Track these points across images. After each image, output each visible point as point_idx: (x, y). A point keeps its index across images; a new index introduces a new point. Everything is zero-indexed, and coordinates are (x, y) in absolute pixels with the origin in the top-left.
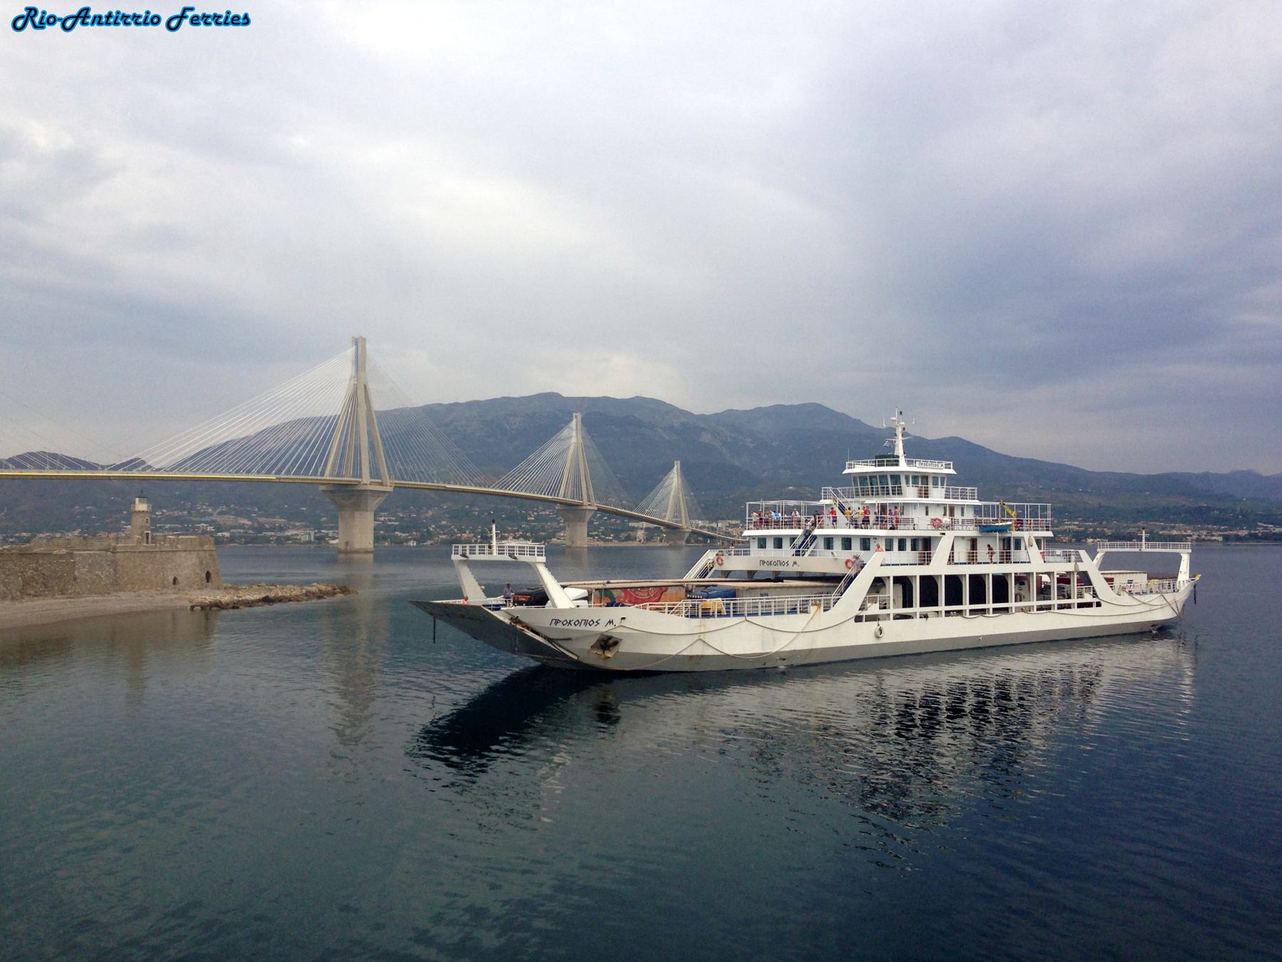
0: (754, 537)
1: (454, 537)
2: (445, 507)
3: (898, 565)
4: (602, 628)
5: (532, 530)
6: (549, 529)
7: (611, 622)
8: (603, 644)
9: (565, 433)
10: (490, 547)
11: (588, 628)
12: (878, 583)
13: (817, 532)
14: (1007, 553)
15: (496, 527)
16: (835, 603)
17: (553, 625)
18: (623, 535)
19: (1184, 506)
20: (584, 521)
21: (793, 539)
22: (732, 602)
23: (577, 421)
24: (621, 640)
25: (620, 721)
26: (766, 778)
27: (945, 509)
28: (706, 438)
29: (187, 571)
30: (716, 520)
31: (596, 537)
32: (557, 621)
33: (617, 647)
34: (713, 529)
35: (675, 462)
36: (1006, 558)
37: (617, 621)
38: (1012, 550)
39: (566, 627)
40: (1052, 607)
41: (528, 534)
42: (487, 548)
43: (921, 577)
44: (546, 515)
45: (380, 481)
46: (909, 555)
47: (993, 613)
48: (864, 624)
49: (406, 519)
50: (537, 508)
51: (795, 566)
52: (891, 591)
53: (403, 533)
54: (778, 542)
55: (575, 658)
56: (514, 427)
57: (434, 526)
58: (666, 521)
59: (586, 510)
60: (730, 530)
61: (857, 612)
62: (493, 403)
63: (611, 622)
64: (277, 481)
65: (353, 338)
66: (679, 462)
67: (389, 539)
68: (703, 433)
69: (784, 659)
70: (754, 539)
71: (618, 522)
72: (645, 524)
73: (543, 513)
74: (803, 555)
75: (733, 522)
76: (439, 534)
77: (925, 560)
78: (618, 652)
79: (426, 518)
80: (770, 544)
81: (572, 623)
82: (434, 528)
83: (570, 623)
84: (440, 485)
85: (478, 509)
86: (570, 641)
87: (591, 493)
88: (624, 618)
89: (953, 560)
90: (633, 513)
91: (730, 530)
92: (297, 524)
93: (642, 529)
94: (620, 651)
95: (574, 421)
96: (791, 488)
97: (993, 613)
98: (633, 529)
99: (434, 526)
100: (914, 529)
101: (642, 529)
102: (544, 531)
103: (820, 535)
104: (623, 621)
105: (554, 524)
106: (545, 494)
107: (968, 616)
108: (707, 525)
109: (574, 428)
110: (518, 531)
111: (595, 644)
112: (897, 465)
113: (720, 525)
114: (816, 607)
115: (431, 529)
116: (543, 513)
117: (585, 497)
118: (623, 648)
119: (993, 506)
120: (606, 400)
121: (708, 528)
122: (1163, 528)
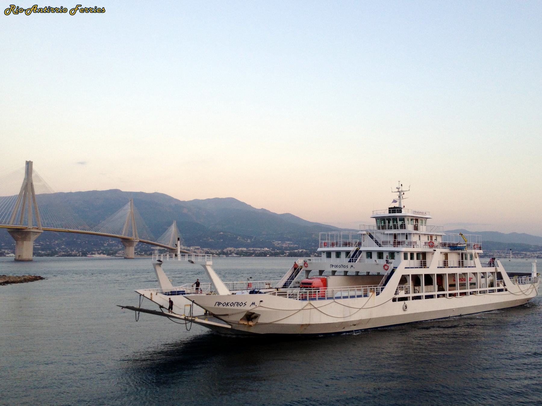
0: (324, 252)
1: (69, 253)
2: (64, 240)
3: (409, 268)
4: (248, 308)
5: (106, 250)
6: (113, 250)
7: (253, 304)
8: (248, 317)
10: (176, 255)
11: (239, 307)
12: (403, 280)
13: (362, 249)
14: (424, 261)
15: (180, 242)
16: (382, 290)
17: (217, 306)
18: (148, 253)
20: (133, 246)
21: (348, 253)
22: (308, 291)
23: (131, 203)
24: (260, 315)
27: (428, 236)
28: (185, 211)
30: (189, 246)
31: (136, 254)
32: (219, 304)
33: (256, 319)
34: (189, 250)
35: (174, 221)
36: (461, 264)
37: (257, 303)
38: (464, 260)
39: (225, 307)
40: (486, 292)
42: (174, 255)
43: (425, 275)
44: (112, 244)
45: (37, 227)
46: (416, 262)
47: (460, 295)
48: (397, 303)
49: (44, 245)
50: (109, 240)
51: (352, 268)
52: (410, 283)
53: (43, 251)
54: (338, 254)
55: (230, 327)
57: (58, 248)
58: (169, 246)
59: (134, 241)
60: (196, 250)
61: (393, 296)
62: (89, 193)
63: (253, 304)
66: (175, 221)
67: (36, 254)
69: (355, 325)
70: (324, 252)
72: (158, 248)
73: (111, 242)
74: (355, 262)
76: (60, 252)
77: (424, 265)
78: (257, 322)
80: (333, 255)
81: (229, 304)
82: (58, 249)
83: (227, 304)
84: (66, 229)
86: (227, 316)
87: (137, 234)
88: (261, 301)
89: (463, 265)
90: (155, 243)
91: (196, 250)
93: (157, 250)
94: (258, 322)
96: (222, 233)
97: (460, 295)
98: (153, 250)
99: (58, 248)
100: (414, 247)
101: (157, 250)
102: (112, 251)
103: (363, 251)
104: (261, 303)
105: (117, 248)
107: (448, 297)
110: (99, 251)
111: (243, 317)
112: (401, 212)
113: (191, 248)
114: (372, 293)
115: (57, 250)
116: (111, 242)
117: (134, 236)
118: (260, 320)
119: (469, 236)
120: (141, 193)
121: (186, 250)
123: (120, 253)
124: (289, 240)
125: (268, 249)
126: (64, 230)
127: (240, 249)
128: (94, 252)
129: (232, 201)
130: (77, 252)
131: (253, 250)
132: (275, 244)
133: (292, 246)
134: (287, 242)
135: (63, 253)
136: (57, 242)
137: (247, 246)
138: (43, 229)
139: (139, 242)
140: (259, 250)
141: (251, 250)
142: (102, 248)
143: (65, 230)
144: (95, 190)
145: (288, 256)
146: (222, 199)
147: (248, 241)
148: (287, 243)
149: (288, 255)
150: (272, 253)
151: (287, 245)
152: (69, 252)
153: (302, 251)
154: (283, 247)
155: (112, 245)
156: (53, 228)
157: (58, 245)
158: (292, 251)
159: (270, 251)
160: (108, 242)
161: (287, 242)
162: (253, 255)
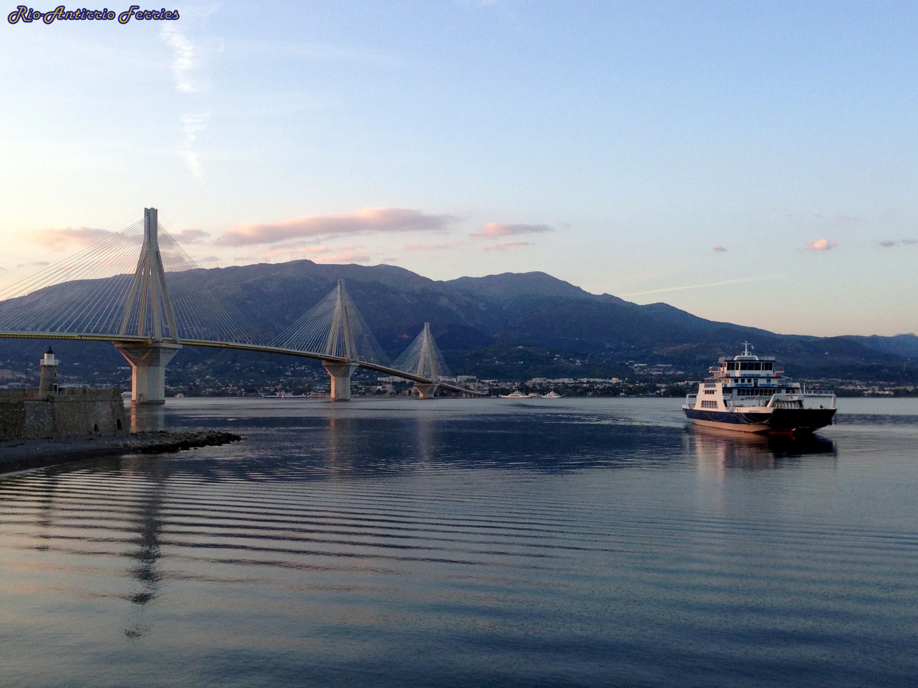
9: (332, 295)
19: (859, 364)
20: (348, 376)
25: (151, 601)
26: (774, 511)
28: (443, 302)
29: (104, 419)
30: (455, 375)
35: (425, 323)
41: (288, 387)
50: (294, 365)
53: (172, 386)
56: (271, 291)
58: (417, 376)
60: (468, 384)
64: (79, 338)
65: (146, 209)
66: (428, 324)
68: (441, 297)
71: (367, 377)
73: (299, 368)
75: (471, 377)
76: (204, 388)
79: (192, 373)
85: (239, 365)
91: (468, 384)
92: (71, 378)
95: (339, 286)
96: (520, 347)
106: (307, 351)
108: (448, 380)
109: (339, 291)
110: (278, 385)
122: (842, 384)
123: (319, 390)
124: (664, 360)
125: (621, 380)
126: (219, 344)
127: (561, 380)
128: (267, 388)
129: (540, 278)
130: (236, 388)
131: (588, 382)
132: (635, 370)
133: (671, 372)
134: (660, 365)
135: (210, 390)
136: (196, 369)
137: (573, 374)
138: (181, 343)
139: (358, 366)
140: (601, 383)
141: (583, 383)
142: (283, 380)
143: (221, 344)
144: (263, 262)
145: (665, 395)
146: (519, 275)
147: (577, 364)
148: (660, 367)
149: (664, 393)
150: (630, 389)
151: (660, 371)
152: (220, 387)
153: (694, 384)
154: (652, 375)
155: (302, 374)
156: (188, 340)
157: (199, 373)
158: (673, 383)
159: (625, 384)
160: (293, 367)
161: (660, 365)
162: (590, 393)
